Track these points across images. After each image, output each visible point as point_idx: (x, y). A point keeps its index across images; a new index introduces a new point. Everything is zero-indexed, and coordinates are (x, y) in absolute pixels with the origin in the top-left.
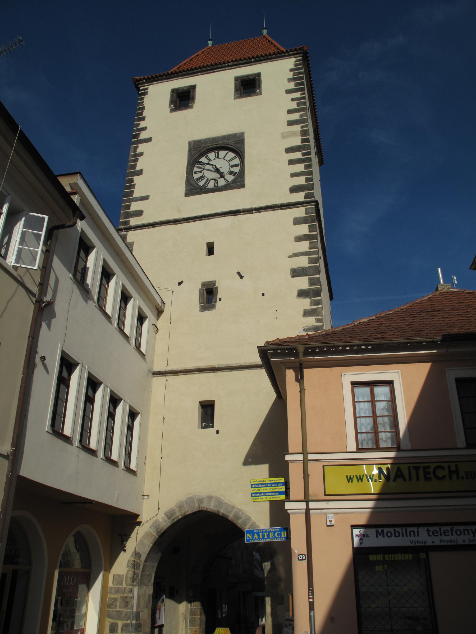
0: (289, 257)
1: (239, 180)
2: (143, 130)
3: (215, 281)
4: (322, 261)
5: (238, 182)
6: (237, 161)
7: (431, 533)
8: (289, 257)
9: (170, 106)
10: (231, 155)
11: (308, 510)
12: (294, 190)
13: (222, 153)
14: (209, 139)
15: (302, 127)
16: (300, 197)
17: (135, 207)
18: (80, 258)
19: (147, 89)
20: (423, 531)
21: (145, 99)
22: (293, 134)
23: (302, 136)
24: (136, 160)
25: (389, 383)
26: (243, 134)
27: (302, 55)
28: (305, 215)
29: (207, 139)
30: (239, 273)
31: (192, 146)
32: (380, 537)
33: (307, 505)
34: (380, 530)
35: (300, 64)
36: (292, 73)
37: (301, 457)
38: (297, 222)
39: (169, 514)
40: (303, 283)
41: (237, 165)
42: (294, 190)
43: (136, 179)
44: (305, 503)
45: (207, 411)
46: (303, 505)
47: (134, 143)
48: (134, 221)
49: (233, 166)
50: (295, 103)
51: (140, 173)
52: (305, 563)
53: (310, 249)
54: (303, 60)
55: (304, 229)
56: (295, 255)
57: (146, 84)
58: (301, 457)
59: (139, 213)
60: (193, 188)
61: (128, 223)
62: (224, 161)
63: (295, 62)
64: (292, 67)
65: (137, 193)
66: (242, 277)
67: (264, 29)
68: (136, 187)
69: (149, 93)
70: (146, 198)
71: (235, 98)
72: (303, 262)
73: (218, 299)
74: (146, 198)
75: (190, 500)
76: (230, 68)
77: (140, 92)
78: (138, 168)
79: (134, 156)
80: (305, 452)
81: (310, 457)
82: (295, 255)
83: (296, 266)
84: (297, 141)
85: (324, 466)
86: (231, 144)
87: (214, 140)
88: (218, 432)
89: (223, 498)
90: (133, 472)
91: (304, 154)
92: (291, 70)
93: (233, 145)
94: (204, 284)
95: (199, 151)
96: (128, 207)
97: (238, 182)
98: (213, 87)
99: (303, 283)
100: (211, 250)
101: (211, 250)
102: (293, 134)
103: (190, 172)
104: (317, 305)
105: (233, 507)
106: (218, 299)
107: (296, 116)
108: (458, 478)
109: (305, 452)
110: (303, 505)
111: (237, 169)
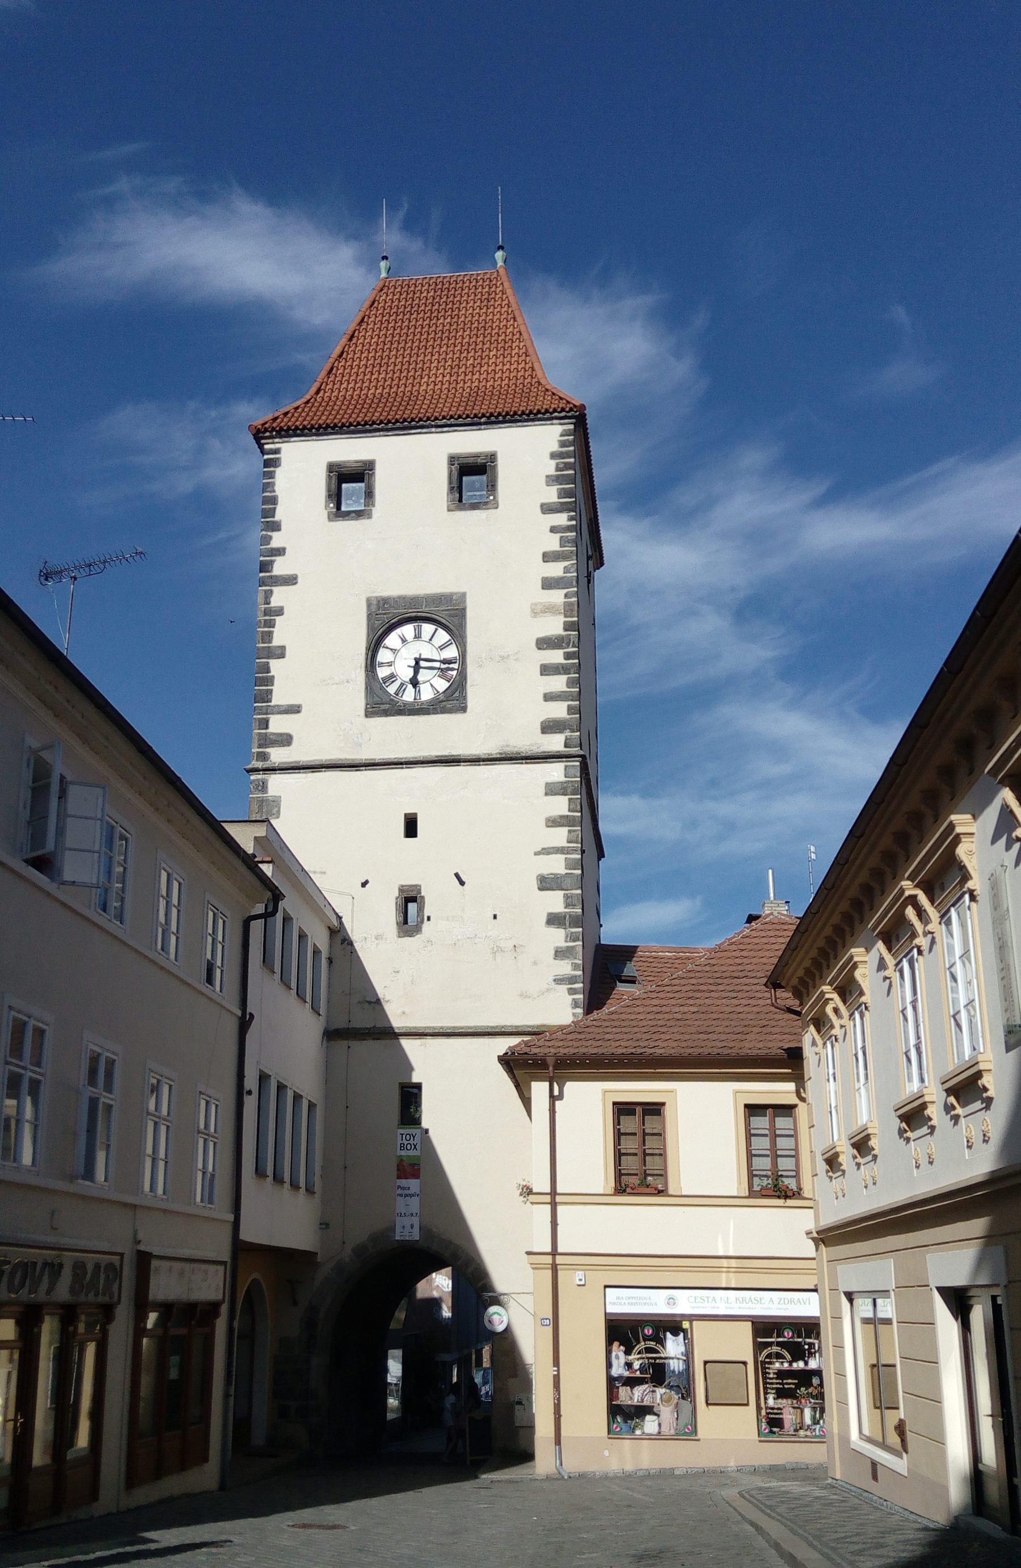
0: (536, 854)
1: (457, 694)
2: (280, 555)
3: (464, 595)
5: (453, 700)
8: (536, 854)
9: (326, 507)
10: (443, 636)
12: (549, 727)
13: (428, 628)
15: (566, 596)
16: (556, 743)
17: (277, 724)
18: (227, 827)
19: (277, 451)
22: (549, 609)
23: (566, 616)
24: (271, 624)
26: (464, 595)
27: (574, 421)
28: (562, 779)
29: (399, 597)
30: (457, 875)
31: (374, 608)
33: (554, 1260)
38: (552, 790)
39: (359, 1251)
42: (549, 727)
43: (276, 666)
44: (550, 1257)
46: (549, 1259)
47: (262, 582)
48: (278, 755)
51: (280, 653)
52: (550, 1329)
53: (568, 842)
54: (574, 432)
56: (546, 851)
57: (277, 440)
59: (285, 740)
60: (381, 703)
61: (264, 757)
62: (430, 642)
63: (561, 435)
64: (555, 447)
65: (280, 696)
66: (462, 883)
69: (283, 462)
72: (557, 865)
73: (426, 918)
74: (294, 710)
76: (440, 430)
78: (276, 642)
79: (266, 613)
82: (546, 851)
83: (546, 871)
84: (555, 626)
85: (606, 1287)
89: (435, 1230)
92: (553, 456)
93: (447, 614)
94: (402, 889)
95: (386, 618)
96: (265, 723)
97: (453, 700)
98: (411, 464)
99: (555, 902)
100: (411, 827)
101: (411, 827)
102: (549, 609)
104: (574, 941)
105: (450, 1242)
106: (426, 918)
110: (549, 1259)
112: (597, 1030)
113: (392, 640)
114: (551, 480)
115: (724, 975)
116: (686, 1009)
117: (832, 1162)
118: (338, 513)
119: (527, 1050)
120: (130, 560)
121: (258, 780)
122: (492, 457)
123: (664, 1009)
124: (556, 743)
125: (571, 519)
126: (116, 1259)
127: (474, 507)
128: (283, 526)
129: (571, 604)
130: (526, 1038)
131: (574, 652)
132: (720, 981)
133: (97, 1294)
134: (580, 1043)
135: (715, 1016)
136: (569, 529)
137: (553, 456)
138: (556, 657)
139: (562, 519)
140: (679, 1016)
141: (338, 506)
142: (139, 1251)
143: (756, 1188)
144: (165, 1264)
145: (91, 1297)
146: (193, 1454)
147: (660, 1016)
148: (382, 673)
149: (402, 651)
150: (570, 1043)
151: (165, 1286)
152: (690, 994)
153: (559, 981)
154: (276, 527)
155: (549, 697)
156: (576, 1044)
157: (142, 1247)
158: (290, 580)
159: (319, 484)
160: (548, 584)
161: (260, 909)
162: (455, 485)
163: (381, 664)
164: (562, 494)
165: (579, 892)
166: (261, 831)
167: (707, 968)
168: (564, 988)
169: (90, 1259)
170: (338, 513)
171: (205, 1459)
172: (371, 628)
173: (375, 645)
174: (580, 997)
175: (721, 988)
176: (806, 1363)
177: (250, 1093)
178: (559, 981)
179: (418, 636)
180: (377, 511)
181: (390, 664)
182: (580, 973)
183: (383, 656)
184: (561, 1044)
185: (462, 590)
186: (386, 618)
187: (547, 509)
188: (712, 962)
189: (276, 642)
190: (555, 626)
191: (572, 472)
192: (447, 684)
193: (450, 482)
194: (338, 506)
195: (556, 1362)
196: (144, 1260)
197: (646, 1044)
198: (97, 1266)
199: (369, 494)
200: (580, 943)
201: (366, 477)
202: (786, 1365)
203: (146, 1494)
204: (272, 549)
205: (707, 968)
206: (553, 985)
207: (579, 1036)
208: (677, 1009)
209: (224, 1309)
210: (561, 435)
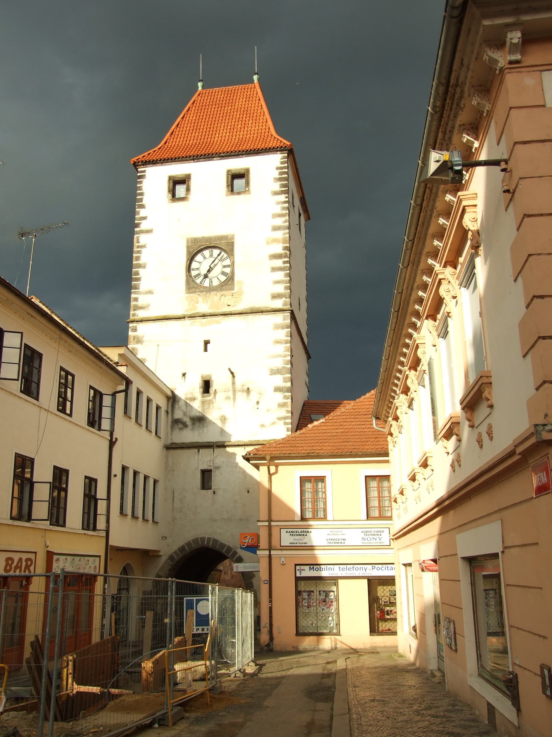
7: (341, 569)
11: (270, 556)
12: (275, 297)
14: (203, 238)
19: (144, 171)
21: (144, 183)
22: (275, 241)
32: (312, 571)
33: (270, 552)
34: (312, 567)
35: (284, 168)
37: (267, 524)
38: (277, 327)
39: (182, 549)
41: (228, 266)
42: (275, 297)
45: (206, 477)
48: (140, 314)
49: (224, 267)
52: (267, 585)
58: (267, 524)
60: (192, 285)
63: (282, 159)
67: (255, 74)
68: (142, 279)
69: (147, 176)
70: (150, 292)
71: (227, 195)
75: (196, 540)
77: (139, 174)
80: (270, 520)
81: (273, 523)
84: (279, 249)
86: (223, 244)
87: (209, 239)
88: (214, 493)
90: (157, 523)
92: (277, 168)
93: (224, 246)
95: (196, 248)
98: (206, 175)
102: (275, 241)
103: (189, 269)
108: (164, 719)
109: (270, 520)
110: (267, 552)
111: (228, 270)
112: (293, 442)
113: (199, 257)
115: (360, 414)
116: (338, 431)
119: (257, 452)
120: (62, 227)
121: (133, 327)
122: (248, 171)
123: (328, 431)
124: (279, 304)
125: (286, 197)
126: (32, 556)
127: (239, 193)
128: (146, 206)
129: (286, 237)
130: (256, 447)
131: (287, 261)
132: (357, 417)
133: (20, 572)
134: (283, 449)
135: (353, 434)
136: (285, 202)
137: (277, 168)
138: (279, 263)
139: (283, 198)
140: (334, 434)
142: (48, 552)
144: (62, 558)
145: (18, 573)
147: (325, 434)
148: (194, 273)
149: (202, 263)
150: (278, 449)
152: (341, 424)
153: (280, 419)
155: (274, 269)
156: (281, 449)
157: (49, 549)
159: (165, 186)
160: (276, 228)
161: (123, 387)
162: (230, 183)
163: (193, 269)
164: (283, 186)
165: (290, 375)
166: (122, 350)
167: (352, 411)
168: (282, 422)
172: (188, 252)
173: (191, 259)
174: (290, 426)
175: (357, 420)
176: (492, 598)
177: (115, 476)
178: (280, 419)
181: (197, 269)
182: (290, 415)
183: (194, 265)
184: (274, 449)
185: (233, 234)
186: (196, 248)
187: (276, 193)
188: (354, 407)
191: (286, 176)
192: (225, 278)
193: (228, 182)
194: (174, 195)
195: (271, 601)
196: (50, 555)
197: (316, 448)
198: (20, 560)
199: (188, 190)
200: (290, 400)
201: (187, 182)
204: (141, 217)
205: (352, 411)
206: (276, 420)
207: (283, 445)
208: (334, 431)
210: (282, 159)
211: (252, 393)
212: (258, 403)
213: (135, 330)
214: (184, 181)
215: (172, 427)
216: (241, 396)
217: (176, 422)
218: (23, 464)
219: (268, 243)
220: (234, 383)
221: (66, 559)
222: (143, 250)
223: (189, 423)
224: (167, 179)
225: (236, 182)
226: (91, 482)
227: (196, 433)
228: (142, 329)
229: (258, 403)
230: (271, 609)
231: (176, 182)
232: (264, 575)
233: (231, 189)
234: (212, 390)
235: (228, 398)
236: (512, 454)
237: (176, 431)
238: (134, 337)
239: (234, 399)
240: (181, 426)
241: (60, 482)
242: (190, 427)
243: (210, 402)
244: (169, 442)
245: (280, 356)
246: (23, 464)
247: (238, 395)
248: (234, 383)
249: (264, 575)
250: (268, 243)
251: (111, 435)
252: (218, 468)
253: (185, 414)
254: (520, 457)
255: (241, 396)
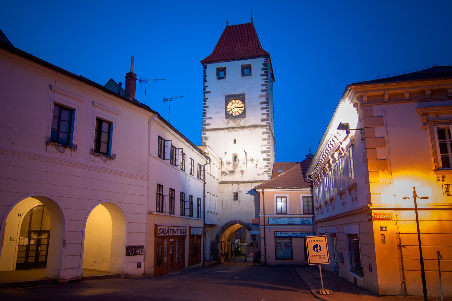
4: (270, 133)
6: (242, 105)
10: (240, 102)
11: (264, 228)
12: (263, 120)
16: (264, 123)
19: (206, 66)
20: (291, 233)
22: (262, 96)
25: (286, 197)
36: (264, 81)
38: (264, 133)
40: (265, 156)
42: (263, 120)
48: (207, 127)
50: (264, 81)
55: (266, 136)
59: (209, 125)
74: (210, 118)
78: (207, 105)
80: (264, 214)
91: (266, 106)
92: (263, 64)
98: (233, 67)
99: (265, 156)
100: (235, 142)
101: (235, 142)
107: (264, 88)
109: (264, 214)
114: (263, 69)
117: (317, 209)
118: (219, 78)
122: (250, 65)
127: (247, 75)
137: (263, 64)
141: (219, 76)
143: (47, 235)
146: (198, 261)
151: (194, 232)
153: (265, 172)
154: (206, 81)
155: (263, 114)
158: (209, 92)
160: (262, 91)
168: (266, 173)
169: (182, 228)
170: (219, 78)
171: (200, 262)
179: (235, 103)
180: (227, 77)
183: (229, 106)
187: (262, 75)
189: (207, 105)
190: (264, 100)
194: (219, 76)
198: (181, 229)
199: (225, 74)
202: (177, 261)
203: (192, 267)
209: (203, 236)
211: (254, 161)
212: (256, 165)
213: (205, 134)
214: (224, 69)
215: (221, 175)
216: (249, 162)
217: (223, 173)
218: (160, 187)
219: (259, 97)
220: (246, 157)
221: (310, 241)
222: (207, 100)
223: (228, 173)
224: (216, 69)
225: (245, 70)
226: (199, 199)
227: (231, 177)
228: (208, 134)
229: (256, 165)
230: (265, 249)
231: (219, 70)
232: (262, 236)
233: (243, 74)
234: (237, 160)
235: (244, 163)
236: (362, 209)
237: (223, 177)
238: (204, 137)
239: (247, 163)
240: (225, 174)
241: (160, 192)
242: (229, 175)
243: (237, 164)
244: (220, 181)
245: (265, 145)
246: (160, 187)
247: (248, 162)
248: (246, 157)
249: (262, 236)
250: (259, 97)
251: (204, 181)
252: (241, 192)
253: (226, 170)
254: (352, 281)
255: (249, 162)
